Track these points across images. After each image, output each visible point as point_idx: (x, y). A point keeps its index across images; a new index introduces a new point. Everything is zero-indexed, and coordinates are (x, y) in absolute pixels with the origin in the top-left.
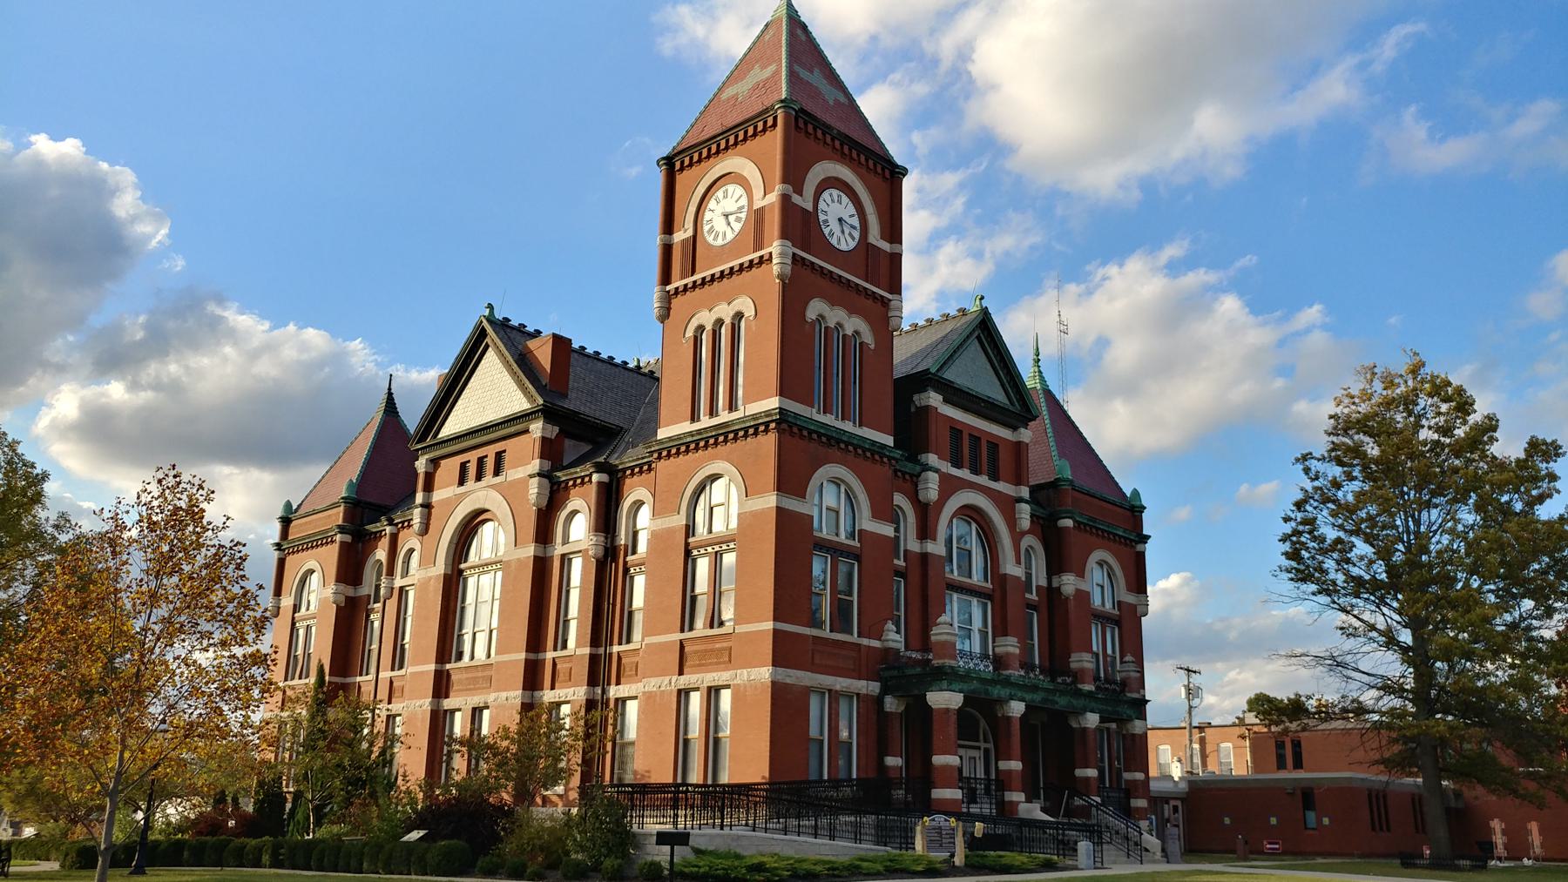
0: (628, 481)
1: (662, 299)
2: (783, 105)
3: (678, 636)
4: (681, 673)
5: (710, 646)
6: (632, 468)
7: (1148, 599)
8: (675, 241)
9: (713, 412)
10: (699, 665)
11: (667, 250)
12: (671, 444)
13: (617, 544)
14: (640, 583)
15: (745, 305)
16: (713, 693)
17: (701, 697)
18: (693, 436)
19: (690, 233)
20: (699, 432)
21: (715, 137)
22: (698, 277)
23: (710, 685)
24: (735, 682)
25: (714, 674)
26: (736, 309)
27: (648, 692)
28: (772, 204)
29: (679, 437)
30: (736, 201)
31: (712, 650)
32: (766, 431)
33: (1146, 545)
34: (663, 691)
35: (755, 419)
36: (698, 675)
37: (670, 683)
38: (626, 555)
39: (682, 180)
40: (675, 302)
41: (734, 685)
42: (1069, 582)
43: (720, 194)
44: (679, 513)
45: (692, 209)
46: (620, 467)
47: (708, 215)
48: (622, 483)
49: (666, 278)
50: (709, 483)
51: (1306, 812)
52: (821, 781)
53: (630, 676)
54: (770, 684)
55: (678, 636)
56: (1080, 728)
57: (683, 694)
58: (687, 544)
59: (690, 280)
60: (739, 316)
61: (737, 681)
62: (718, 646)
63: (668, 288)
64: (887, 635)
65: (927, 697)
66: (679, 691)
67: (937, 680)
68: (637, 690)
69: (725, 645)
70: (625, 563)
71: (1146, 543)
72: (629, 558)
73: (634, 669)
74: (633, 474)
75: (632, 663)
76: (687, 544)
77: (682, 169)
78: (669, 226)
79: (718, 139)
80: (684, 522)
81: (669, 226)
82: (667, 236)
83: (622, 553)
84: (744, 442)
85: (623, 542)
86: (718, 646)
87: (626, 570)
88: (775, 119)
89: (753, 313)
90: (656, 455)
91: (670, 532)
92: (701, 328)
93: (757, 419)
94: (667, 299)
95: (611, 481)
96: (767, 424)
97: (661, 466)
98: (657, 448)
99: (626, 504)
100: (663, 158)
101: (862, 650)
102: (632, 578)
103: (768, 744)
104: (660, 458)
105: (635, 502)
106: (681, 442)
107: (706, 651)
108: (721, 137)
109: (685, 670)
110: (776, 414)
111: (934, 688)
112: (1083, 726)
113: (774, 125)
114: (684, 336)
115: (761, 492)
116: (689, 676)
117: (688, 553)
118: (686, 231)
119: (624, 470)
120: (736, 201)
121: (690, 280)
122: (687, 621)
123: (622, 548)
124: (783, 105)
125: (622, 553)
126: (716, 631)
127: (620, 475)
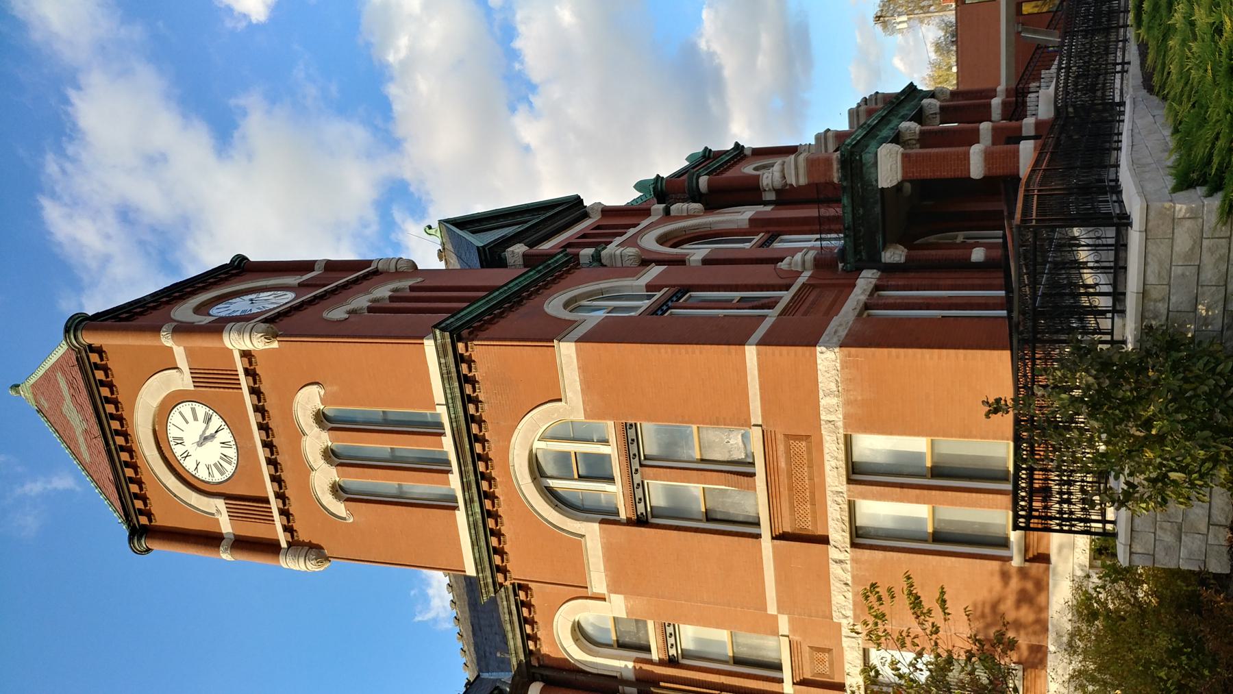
0: (545, 650)
1: (296, 556)
2: (72, 332)
3: (766, 543)
4: (824, 540)
5: (784, 479)
6: (526, 638)
7: (803, 144)
8: (230, 531)
9: (438, 466)
10: (813, 504)
11: (242, 544)
12: (483, 543)
13: (630, 676)
14: (689, 636)
15: (308, 401)
16: (857, 472)
17: (865, 497)
18: (472, 501)
19: (220, 503)
20: (468, 502)
21: (109, 452)
22: (270, 489)
23: (844, 479)
24: (840, 424)
25: (827, 468)
26: (311, 421)
27: (854, 610)
28: (190, 354)
29: (472, 526)
30: (187, 422)
31: (790, 476)
32: (470, 362)
33: (745, 147)
34: (853, 577)
35: (450, 379)
36: (829, 503)
37: (841, 562)
38: (650, 662)
39: (162, 519)
40: (303, 536)
41: (846, 426)
42: (770, 178)
43: (178, 450)
44: (583, 536)
45: (194, 499)
46: (522, 657)
47: (189, 464)
48: (547, 662)
49: (270, 547)
50: (544, 480)
51: (1005, 523)
52: (1007, 304)
53: (831, 664)
54: (846, 350)
55: (766, 543)
56: (940, 113)
57: (860, 537)
58: (629, 522)
59: (274, 505)
60: (322, 419)
61: (838, 418)
62: (783, 464)
63: (284, 545)
64: (796, 265)
65: (885, 186)
66: (854, 545)
67: (861, 168)
68: (852, 648)
69: (781, 448)
70: (661, 663)
71: (743, 146)
72: (655, 656)
73: (820, 655)
74: (534, 638)
75: (812, 658)
76: (629, 522)
77: (149, 515)
78: (211, 539)
79: (113, 447)
80: (596, 526)
81: (211, 539)
82: (224, 542)
83: (646, 667)
84: (486, 406)
85: (630, 665)
86: (783, 464)
87: (672, 662)
88: (91, 348)
89: (315, 387)
90: (500, 577)
91: (611, 554)
92: (338, 490)
93: (449, 373)
94: (297, 546)
95: (543, 679)
96: (460, 359)
97: (518, 570)
98: (488, 573)
99: (576, 654)
100: (131, 540)
101: (812, 282)
102: (686, 654)
103: (944, 352)
104: (503, 570)
105: (576, 640)
106: (480, 524)
107: (791, 489)
108: (111, 442)
109: (820, 532)
110: (443, 338)
111: (873, 177)
112: (938, 111)
113: (100, 351)
114: (344, 519)
115: (552, 369)
116: (831, 523)
117: (640, 522)
118: (218, 511)
119: (529, 653)
120: (187, 422)
121: (274, 505)
122: (746, 528)
123: (638, 666)
124: (72, 332)
125: (646, 667)
126: (760, 469)
127: (534, 662)
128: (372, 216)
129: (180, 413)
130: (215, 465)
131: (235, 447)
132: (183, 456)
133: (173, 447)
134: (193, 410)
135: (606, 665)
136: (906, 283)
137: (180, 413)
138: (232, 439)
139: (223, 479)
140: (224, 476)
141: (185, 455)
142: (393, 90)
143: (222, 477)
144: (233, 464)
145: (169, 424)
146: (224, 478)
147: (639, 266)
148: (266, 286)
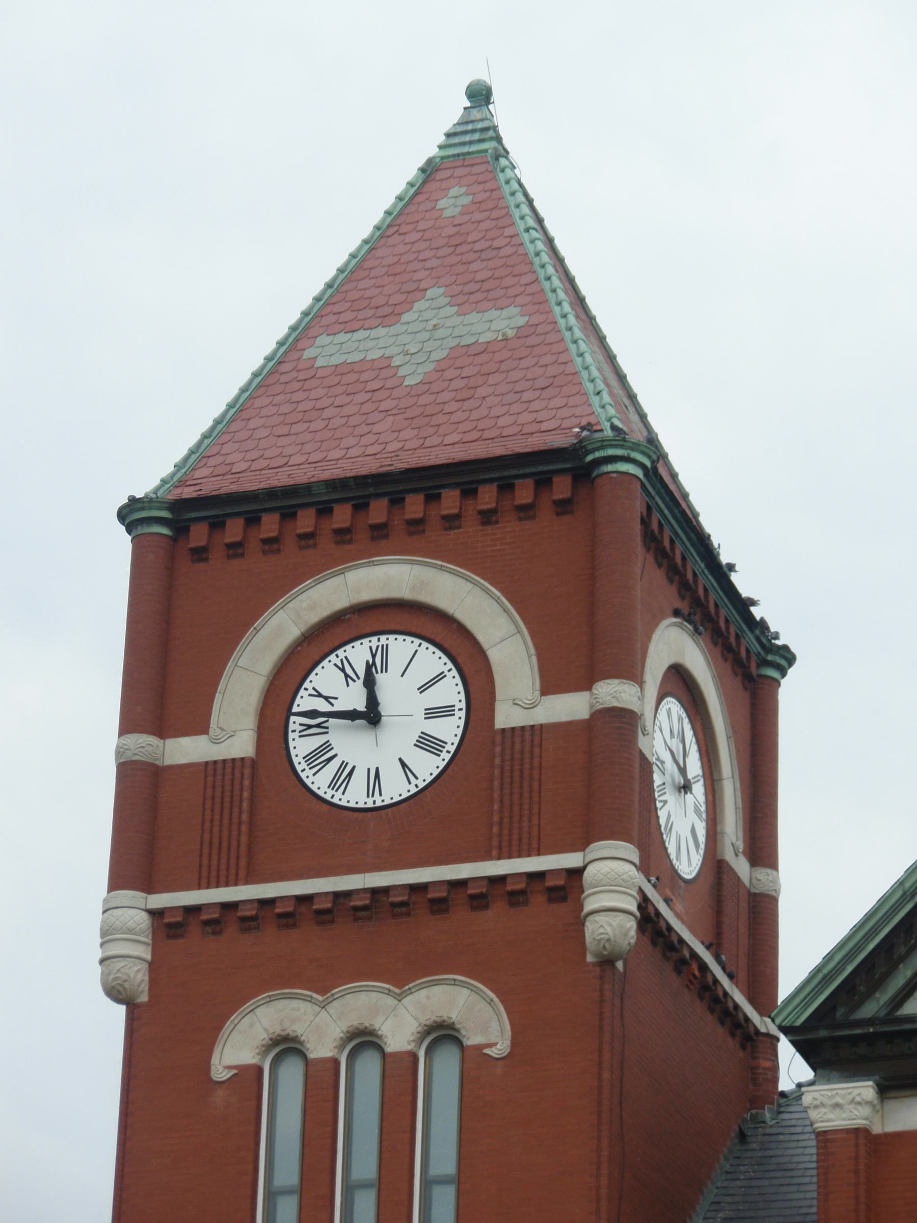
30: (423, 689)
120: (423, 689)
128: (816, 1083)
129: (440, 677)
130: (327, 746)
131: (370, 805)
132: (345, 661)
133: (365, 641)
134: (446, 711)
135: (264, 1199)
136: (674, 507)
137: (440, 677)
138: (388, 801)
139: (296, 761)
140: (304, 765)
141: (349, 670)
142: (380, 1033)
143: (300, 759)
144: (330, 792)
145: (417, 641)
146: (300, 764)
147: (584, 868)
148: (721, 780)
